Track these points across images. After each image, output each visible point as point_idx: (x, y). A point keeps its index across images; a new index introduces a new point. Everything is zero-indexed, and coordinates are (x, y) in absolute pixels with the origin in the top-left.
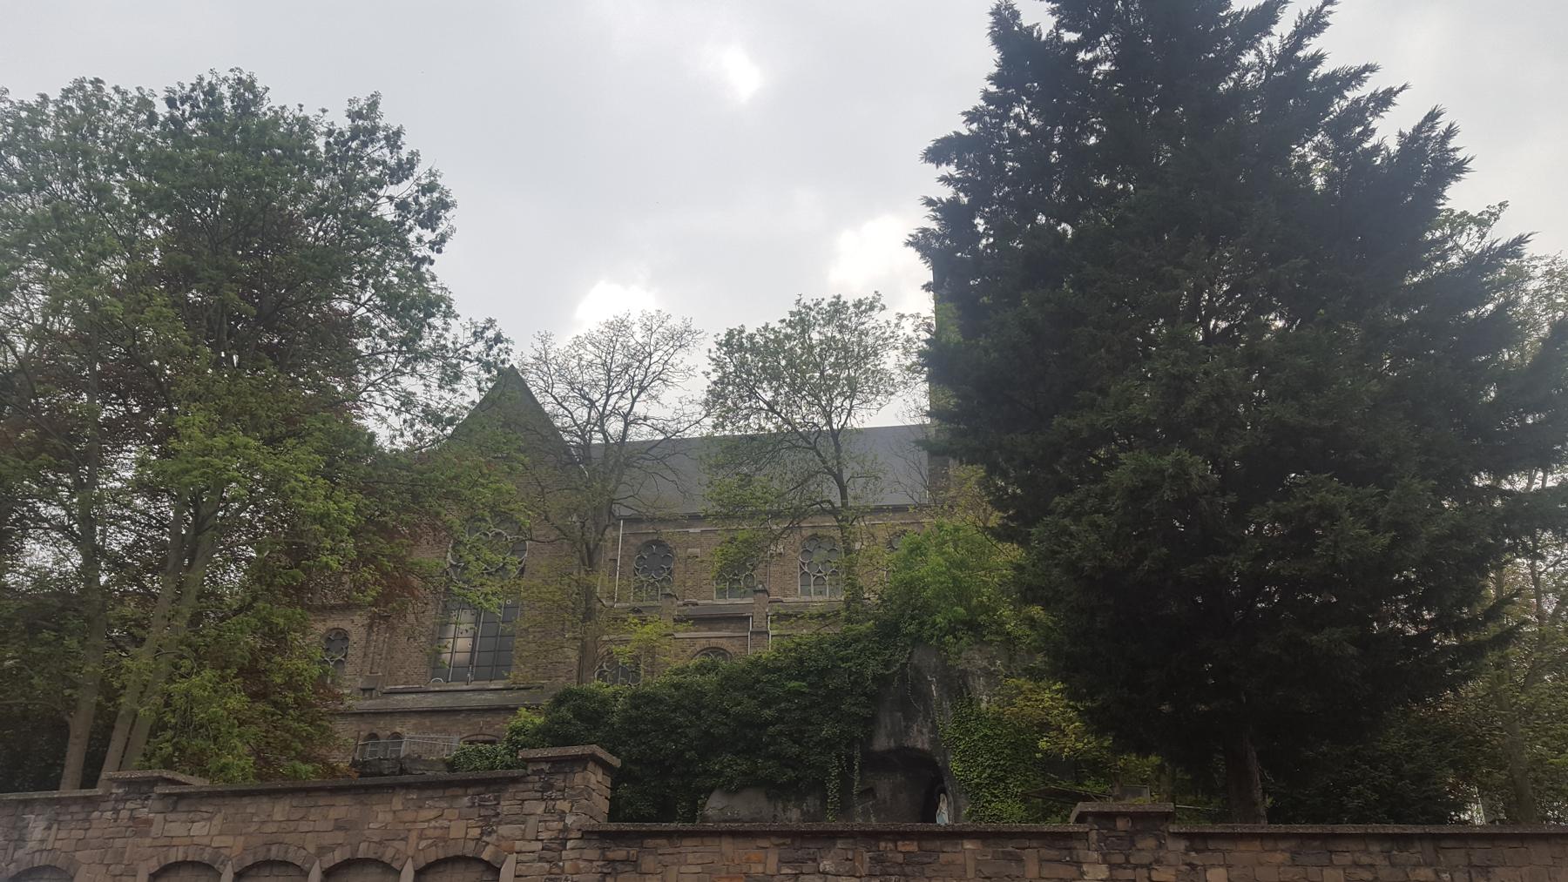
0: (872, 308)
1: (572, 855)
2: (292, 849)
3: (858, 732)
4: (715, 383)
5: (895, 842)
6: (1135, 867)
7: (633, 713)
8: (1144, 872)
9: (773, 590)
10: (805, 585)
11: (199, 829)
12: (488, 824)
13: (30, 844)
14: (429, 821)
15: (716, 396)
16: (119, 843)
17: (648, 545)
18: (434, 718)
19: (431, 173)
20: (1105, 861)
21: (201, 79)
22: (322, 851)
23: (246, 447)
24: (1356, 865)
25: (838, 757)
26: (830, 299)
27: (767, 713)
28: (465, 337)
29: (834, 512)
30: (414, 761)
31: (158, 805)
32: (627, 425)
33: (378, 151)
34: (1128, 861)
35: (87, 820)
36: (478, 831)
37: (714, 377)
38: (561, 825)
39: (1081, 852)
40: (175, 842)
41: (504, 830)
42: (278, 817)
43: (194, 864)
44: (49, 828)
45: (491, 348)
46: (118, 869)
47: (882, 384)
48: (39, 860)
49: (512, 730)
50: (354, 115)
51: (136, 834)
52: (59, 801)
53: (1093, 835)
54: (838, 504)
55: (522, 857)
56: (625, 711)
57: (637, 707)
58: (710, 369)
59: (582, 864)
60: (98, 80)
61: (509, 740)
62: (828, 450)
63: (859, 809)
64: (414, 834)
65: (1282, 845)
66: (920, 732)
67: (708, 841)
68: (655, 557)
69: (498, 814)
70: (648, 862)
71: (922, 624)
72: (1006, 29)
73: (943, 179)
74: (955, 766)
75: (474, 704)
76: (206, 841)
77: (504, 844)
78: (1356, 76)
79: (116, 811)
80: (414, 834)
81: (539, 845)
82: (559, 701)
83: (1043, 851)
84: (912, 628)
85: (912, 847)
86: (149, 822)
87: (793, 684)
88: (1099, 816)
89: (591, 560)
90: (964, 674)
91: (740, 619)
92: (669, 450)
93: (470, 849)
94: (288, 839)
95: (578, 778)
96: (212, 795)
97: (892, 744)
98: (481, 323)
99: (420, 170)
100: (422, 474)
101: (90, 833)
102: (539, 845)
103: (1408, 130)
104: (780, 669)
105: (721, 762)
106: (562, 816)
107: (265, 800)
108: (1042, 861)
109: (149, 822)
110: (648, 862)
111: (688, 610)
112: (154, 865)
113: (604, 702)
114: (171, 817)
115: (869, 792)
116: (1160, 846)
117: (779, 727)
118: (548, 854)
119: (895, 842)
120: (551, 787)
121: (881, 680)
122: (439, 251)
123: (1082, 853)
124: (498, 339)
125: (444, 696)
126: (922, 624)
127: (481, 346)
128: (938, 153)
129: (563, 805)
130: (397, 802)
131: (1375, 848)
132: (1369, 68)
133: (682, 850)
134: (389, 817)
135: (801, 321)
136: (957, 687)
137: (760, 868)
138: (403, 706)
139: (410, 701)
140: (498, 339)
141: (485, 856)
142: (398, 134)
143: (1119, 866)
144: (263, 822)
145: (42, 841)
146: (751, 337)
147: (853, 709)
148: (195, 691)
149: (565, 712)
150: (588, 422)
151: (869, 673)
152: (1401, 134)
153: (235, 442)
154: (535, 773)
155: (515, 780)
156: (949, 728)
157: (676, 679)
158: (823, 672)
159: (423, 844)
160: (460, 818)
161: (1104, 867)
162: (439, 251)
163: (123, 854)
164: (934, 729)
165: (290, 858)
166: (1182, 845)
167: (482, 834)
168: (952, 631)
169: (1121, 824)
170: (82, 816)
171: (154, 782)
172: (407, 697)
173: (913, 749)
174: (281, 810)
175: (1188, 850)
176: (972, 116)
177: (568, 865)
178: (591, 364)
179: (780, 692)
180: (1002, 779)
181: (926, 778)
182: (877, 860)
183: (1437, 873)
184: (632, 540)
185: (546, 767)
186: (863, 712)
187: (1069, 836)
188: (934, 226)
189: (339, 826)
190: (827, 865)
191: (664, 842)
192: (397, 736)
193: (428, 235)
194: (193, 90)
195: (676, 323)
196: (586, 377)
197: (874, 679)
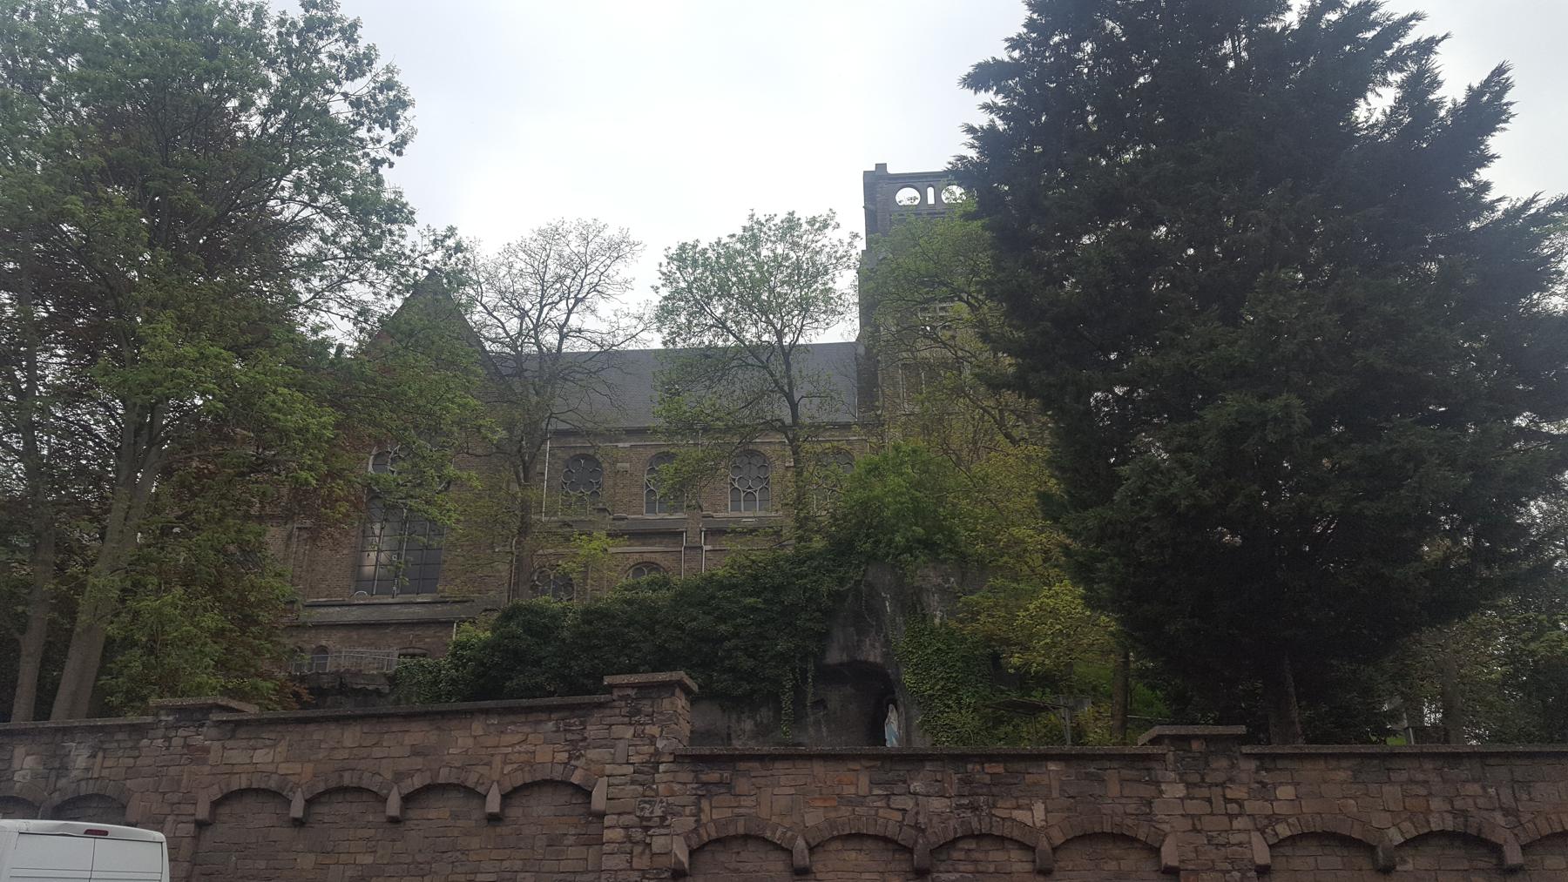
0: (826, 226)
1: (666, 777)
2: (367, 775)
4: (665, 298)
6: (1210, 786)
7: (587, 628)
8: (1219, 789)
9: (705, 505)
11: (260, 756)
13: (75, 773)
14: (513, 745)
15: (665, 313)
16: (173, 771)
17: (576, 459)
18: (362, 632)
19: (389, 70)
20: (1182, 781)
22: (399, 777)
23: (216, 357)
24: (1412, 781)
25: (793, 670)
26: (782, 215)
27: (722, 628)
28: (424, 245)
29: (783, 429)
31: (214, 732)
33: (331, 46)
34: (1203, 780)
37: (665, 292)
38: (652, 749)
39: (1159, 773)
41: (592, 754)
42: (348, 743)
43: (258, 791)
44: (93, 756)
45: (450, 257)
46: (175, 798)
47: (830, 304)
48: (85, 789)
54: (788, 420)
55: (612, 780)
56: (578, 626)
57: (590, 623)
58: (659, 283)
59: (676, 787)
61: (454, 655)
62: (778, 367)
63: (812, 718)
64: (498, 760)
65: (1345, 764)
66: (873, 646)
68: (585, 469)
69: (585, 739)
70: (742, 785)
71: (877, 542)
73: (986, 107)
74: (907, 678)
75: (403, 617)
76: (271, 768)
77: (594, 767)
78: (1404, 25)
79: (168, 739)
80: (498, 760)
82: (508, 616)
83: (1123, 772)
85: (999, 768)
86: (207, 750)
88: (1175, 739)
91: (676, 535)
92: (610, 362)
95: (666, 703)
96: (260, 723)
97: (845, 658)
98: (441, 230)
99: (379, 66)
100: (389, 388)
103: (1476, 85)
104: (735, 586)
106: (652, 740)
107: (332, 726)
108: (1123, 781)
109: (207, 750)
110: (742, 785)
111: (623, 525)
112: (215, 793)
113: (554, 617)
114: (229, 744)
115: (820, 703)
116: (1233, 766)
120: (639, 712)
121: (837, 597)
122: (400, 154)
123: (1160, 773)
124: (459, 248)
125: (370, 609)
126: (877, 542)
127: (438, 255)
128: (981, 77)
129: (653, 730)
130: (477, 727)
131: (1428, 765)
132: (1416, 16)
133: (774, 772)
134: (470, 742)
135: (752, 237)
136: (912, 604)
137: (852, 790)
138: (327, 619)
139: (334, 615)
140: (459, 248)
141: (575, 779)
142: (354, 26)
143: (1195, 785)
145: (87, 769)
146: (704, 251)
149: (514, 627)
150: (520, 334)
151: (824, 589)
152: (1470, 88)
153: (207, 352)
154: (621, 698)
155: (600, 706)
157: (628, 595)
158: (777, 589)
159: (508, 768)
161: (1181, 786)
162: (400, 154)
163: (179, 782)
164: (887, 642)
167: (570, 758)
168: (909, 549)
169: (1196, 745)
170: (130, 744)
172: (331, 610)
173: (866, 662)
174: (351, 736)
176: (1015, 43)
177: (661, 787)
178: (522, 274)
181: (877, 691)
182: (967, 781)
183: (1484, 788)
184: (559, 453)
185: (632, 693)
187: (1147, 757)
188: (972, 154)
189: (416, 752)
190: (916, 786)
191: (757, 765)
192: (323, 650)
193: (388, 136)
195: (612, 232)
196: (517, 286)
197: (830, 595)
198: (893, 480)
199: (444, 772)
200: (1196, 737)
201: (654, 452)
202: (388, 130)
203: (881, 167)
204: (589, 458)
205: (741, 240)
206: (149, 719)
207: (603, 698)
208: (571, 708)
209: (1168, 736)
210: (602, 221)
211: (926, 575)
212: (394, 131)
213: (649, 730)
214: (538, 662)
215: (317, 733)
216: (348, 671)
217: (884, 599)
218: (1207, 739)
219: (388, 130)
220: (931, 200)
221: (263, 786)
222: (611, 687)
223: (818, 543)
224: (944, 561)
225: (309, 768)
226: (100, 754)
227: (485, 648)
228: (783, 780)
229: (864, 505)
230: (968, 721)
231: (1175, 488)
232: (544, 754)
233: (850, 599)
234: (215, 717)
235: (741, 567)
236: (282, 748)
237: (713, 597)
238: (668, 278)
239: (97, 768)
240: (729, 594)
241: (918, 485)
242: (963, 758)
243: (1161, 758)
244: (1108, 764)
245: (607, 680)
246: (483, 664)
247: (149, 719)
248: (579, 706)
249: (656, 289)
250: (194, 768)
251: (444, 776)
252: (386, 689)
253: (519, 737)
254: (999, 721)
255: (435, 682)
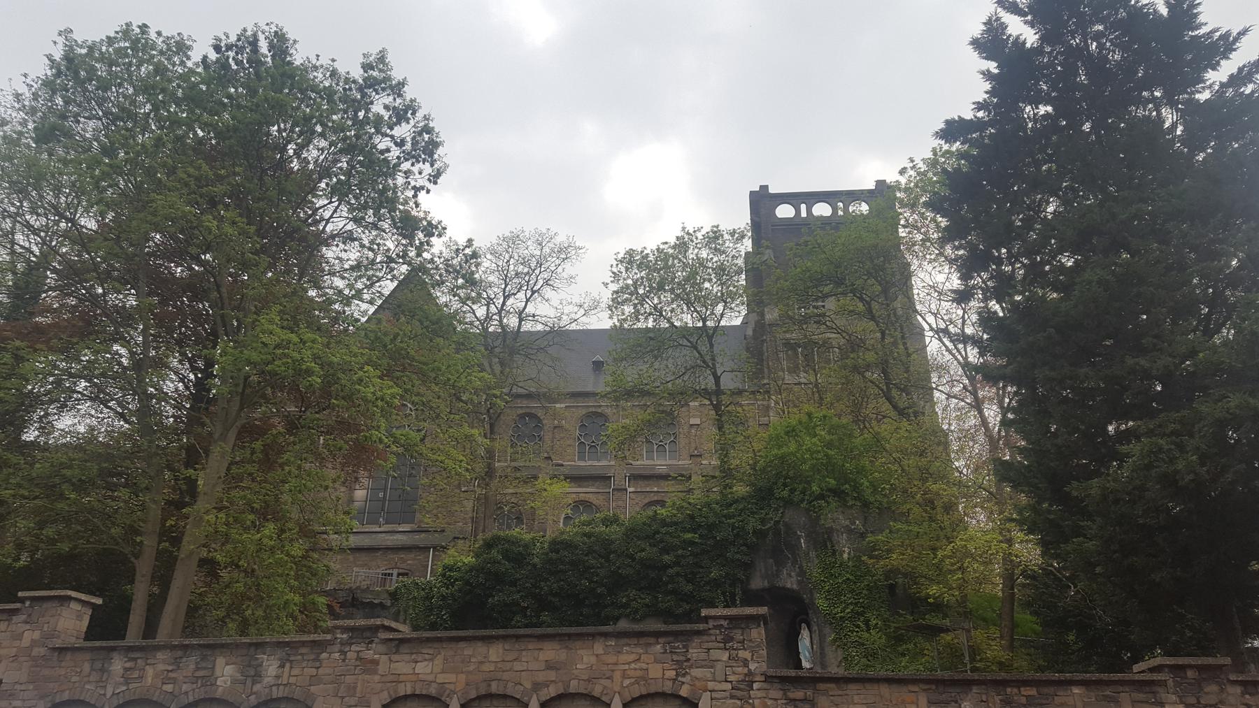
2: (510, 685)
3: (741, 575)
5: (1019, 688)
7: (554, 556)
10: (650, 452)
11: (423, 668)
12: (682, 667)
13: (266, 680)
14: (629, 663)
16: (349, 679)
20: (1182, 703)
21: (245, 30)
22: (537, 687)
23: (313, 341)
25: (724, 594)
26: (707, 229)
30: (364, 591)
31: (382, 648)
32: (521, 320)
35: (317, 659)
36: (674, 673)
37: (614, 287)
38: (746, 670)
39: (1163, 696)
40: (402, 678)
41: (696, 672)
42: (493, 658)
48: (276, 693)
49: (445, 567)
50: (367, 67)
51: (364, 671)
52: (288, 644)
53: (1170, 683)
57: (557, 552)
60: (145, 26)
61: (443, 575)
64: (617, 675)
67: (868, 686)
69: (688, 660)
72: (991, 42)
74: (821, 602)
75: (389, 543)
76: (431, 678)
81: (729, 686)
82: (489, 545)
84: (785, 493)
86: (376, 662)
87: (689, 536)
89: (492, 432)
90: (830, 531)
92: (557, 337)
93: (668, 687)
94: (506, 676)
97: (766, 584)
99: (420, 115)
101: (321, 671)
102: (729, 686)
104: (676, 524)
105: (628, 596)
106: (745, 663)
107: (480, 644)
108: (1134, 702)
109: (376, 662)
112: (385, 698)
113: (526, 546)
116: (1222, 690)
117: (676, 569)
118: (739, 693)
119: (1019, 688)
120: (732, 639)
121: (760, 534)
122: (435, 183)
125: (361, 536)
126: (792, 491)
128: (952, 130)
129: (745, 654)
130: (599, 647)
134: (593, 660)
135: (681, 246)
136: (823, 541)
142: (402, 84)
144: (482, 663)
145: (277, 677)
147: (738, 556)
148: (265, 541)
151: (750, 528)
153: (305, 338)
154: (715, 627)
155: (699, 633)
156: (815, 572)
157: (587, 529)
158: (711, 527)
159: (626, 682)
160: (656, 661)
162: (435, 183)
163: (355, 688)
164: (802, 573)
165: (509, 692)
166: (1238, 690)
167: (677, 675)
168: (822, 497)
169: (1190, 674)
170: (312, 657)
171: (375, 629)
173: (784, 588)
174: (495, 652)
175: (1243, 694)
176: (980, 106)
179: (676, 541)
180: (862, 614)
181: (790, 613)
185: (725, 623)
186: (746, 559)
189: (549, 666)
191: (832, 686)
193: (427, 169)
194: (239, 40)
195: (561, 239)
197: (754, 532)
198: (808, 441)
199: (574, 683)
200: (1190, 666)
201: (584, 411)
202: (427, 165)
203: (764, 188)
204: (532, 416)
205: (674, 247)
206: (329, 637)
207: (701, 627)
208: (676, 635)
209: (1167, 666)
210: (554, 230)
211: (836, 518)
212: (432, 165)
213: (742, 654)
214: (513, 583)
215: (467, 650)
216: (358, 588)
217: (799, 538)
218: (1200, 668)
219: (427, 165)
220: (804, 214)
221: (424, 692)
222: (707, 619)
223: (740, 490)
224: (851, 507)
225: (462, 677)
226: (288, 665)
227: (471, 570)
228: (856, 699)
229: (782, 458)
230: (876, 638)
231: (1180, 465)
232: (655, 671)
233: (770, 536)
234: (383, 635)
235: (680, 508)
236: (439, 661)
237: (658, 532)
238: (616, 276)
239: (286, 675)
240: (671, 529)
241: (829, 445)
242: (1004, 683)
243: (1163, 684)
244: (1121, 689)
245: (704, 612)
246: (471, 584)
247: (329, 637)
248: (682, 633)
249: (606, 285)
250: (367, 677)
251: (574, 687)
252: (389, 603)
253: (633, 657)
254: (899, 639)
255: (428, 598)
